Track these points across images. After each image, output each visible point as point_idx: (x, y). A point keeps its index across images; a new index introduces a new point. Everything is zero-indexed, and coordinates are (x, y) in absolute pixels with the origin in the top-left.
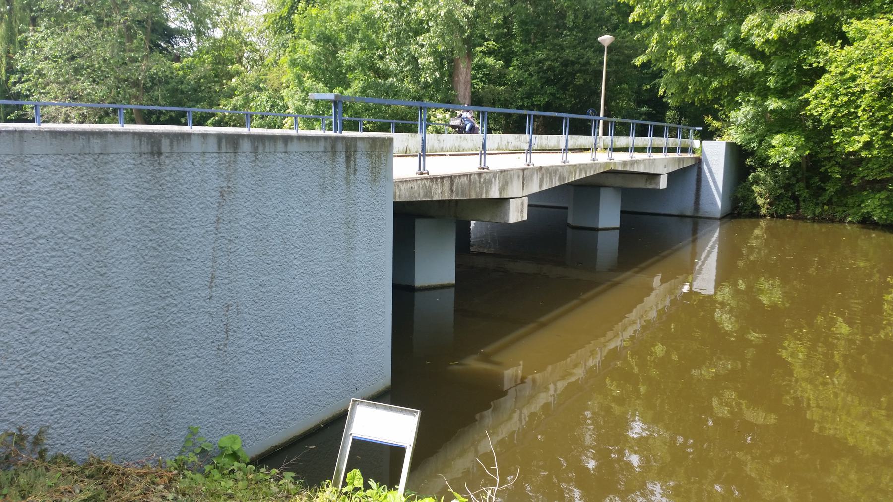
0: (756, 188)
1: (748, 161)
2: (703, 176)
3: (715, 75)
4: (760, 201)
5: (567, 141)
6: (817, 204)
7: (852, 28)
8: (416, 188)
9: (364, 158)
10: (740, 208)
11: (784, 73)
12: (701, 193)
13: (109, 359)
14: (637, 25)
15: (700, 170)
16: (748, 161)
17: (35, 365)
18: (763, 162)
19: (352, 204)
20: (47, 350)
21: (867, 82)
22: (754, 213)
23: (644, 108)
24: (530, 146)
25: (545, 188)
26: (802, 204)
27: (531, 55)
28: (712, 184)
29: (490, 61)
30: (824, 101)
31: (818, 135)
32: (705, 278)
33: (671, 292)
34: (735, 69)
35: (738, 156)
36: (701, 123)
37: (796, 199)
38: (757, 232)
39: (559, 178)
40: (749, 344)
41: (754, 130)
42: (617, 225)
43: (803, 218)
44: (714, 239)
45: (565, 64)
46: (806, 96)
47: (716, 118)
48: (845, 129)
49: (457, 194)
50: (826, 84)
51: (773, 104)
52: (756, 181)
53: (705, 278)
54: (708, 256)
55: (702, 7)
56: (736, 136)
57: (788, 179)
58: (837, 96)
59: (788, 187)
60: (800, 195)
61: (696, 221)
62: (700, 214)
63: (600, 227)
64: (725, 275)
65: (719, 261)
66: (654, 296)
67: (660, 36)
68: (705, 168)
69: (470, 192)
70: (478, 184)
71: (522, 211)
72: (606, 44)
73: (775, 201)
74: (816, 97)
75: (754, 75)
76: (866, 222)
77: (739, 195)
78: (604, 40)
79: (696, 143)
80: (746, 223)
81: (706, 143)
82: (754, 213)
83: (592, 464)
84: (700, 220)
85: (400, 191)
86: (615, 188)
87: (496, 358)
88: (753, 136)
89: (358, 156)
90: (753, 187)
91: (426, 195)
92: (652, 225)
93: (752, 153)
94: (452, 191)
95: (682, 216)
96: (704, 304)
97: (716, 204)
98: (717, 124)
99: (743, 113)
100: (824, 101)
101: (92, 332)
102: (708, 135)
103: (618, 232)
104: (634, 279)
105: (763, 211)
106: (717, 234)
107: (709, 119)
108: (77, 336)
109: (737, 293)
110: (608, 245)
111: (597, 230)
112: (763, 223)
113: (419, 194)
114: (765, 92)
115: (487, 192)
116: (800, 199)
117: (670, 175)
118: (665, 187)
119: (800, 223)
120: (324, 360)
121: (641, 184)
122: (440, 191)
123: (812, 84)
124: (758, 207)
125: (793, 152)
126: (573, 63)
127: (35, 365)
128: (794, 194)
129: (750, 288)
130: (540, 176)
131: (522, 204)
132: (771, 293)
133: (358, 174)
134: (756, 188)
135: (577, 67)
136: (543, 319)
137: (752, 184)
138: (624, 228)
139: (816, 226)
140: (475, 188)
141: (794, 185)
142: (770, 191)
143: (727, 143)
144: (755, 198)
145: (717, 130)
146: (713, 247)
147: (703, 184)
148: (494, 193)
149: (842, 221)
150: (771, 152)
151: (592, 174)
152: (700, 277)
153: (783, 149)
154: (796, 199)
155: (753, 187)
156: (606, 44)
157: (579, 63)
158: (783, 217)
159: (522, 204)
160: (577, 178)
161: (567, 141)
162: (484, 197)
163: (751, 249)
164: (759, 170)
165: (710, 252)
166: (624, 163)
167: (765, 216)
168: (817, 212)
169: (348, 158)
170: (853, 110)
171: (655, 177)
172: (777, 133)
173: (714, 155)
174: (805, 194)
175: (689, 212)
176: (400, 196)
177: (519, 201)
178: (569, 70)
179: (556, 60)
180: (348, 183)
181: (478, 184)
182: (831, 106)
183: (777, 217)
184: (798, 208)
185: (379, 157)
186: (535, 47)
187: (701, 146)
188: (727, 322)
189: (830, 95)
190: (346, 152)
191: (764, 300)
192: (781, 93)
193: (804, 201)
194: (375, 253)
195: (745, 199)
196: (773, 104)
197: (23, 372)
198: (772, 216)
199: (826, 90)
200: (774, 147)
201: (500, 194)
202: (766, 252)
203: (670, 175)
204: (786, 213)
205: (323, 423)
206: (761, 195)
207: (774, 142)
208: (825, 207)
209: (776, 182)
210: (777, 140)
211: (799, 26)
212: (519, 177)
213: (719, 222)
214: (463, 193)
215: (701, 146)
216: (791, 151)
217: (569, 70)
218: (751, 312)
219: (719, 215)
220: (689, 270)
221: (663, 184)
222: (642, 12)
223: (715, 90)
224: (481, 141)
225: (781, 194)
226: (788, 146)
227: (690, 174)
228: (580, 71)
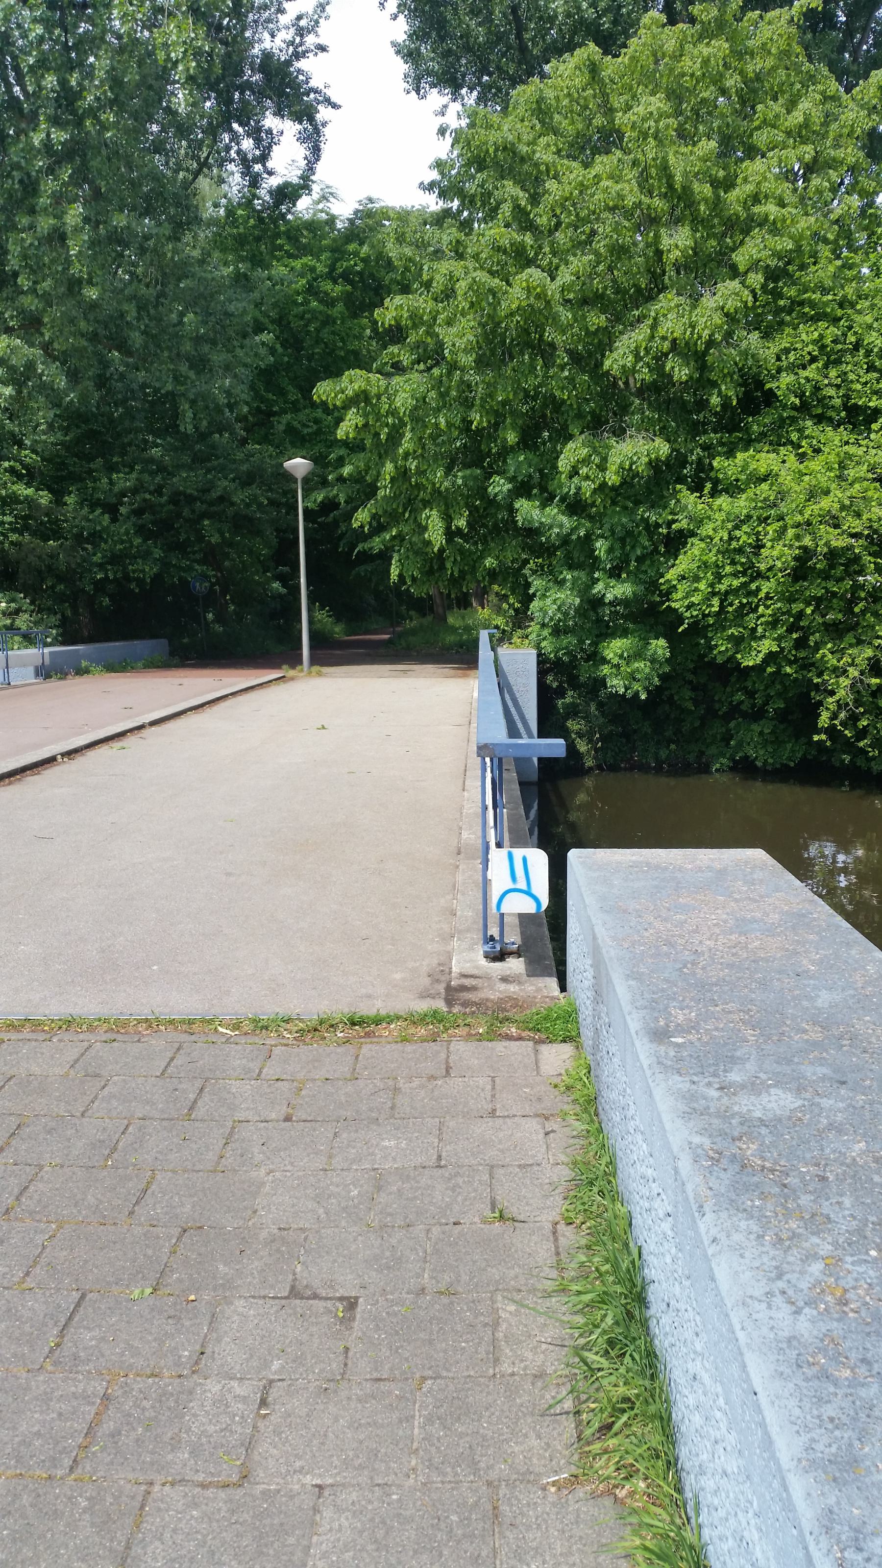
7: (726, 467)
14: (354, 447)
21: (778, 554)
31: (688, 637)
45: (177, 498)
48: (732, 631)
55: (481, 421)
58: (719, 577)
67: (396, 467)
72: (300, 474)
76: (745, 769)
78: (296, 466)
112: (589, 782)
126: (190, 499)
149: (705, 769)
155: (569, 724)
156: (300, 474)
166: (514, 992)
167: (591, 769)
170: (745, 601)
179: (159, 491)
182: (714, 594)
208: (673, 746)
211: (650, 463)
222: (360, 421)
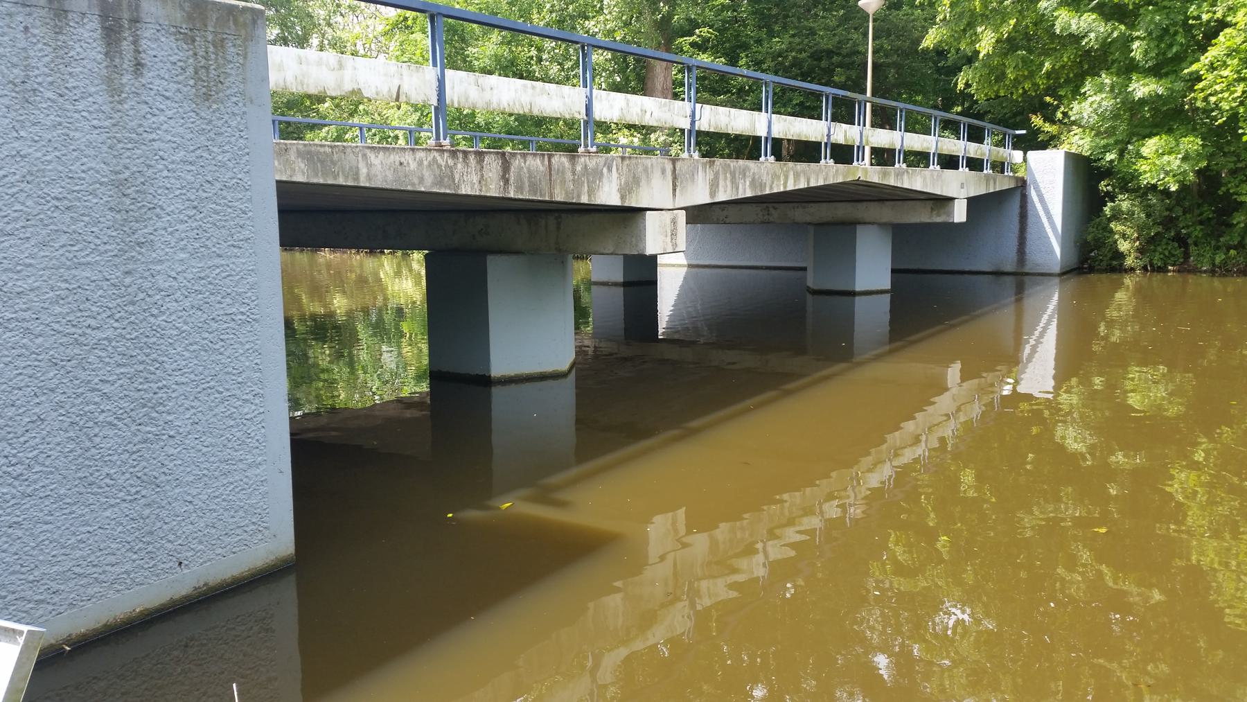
0: (1116, 226)
1: (1103, 186)
2: (1029, 207)
3: (1046, 53)
4: (1124, 246)
5: (770, 123)
6: (1217, 248)
8: (413, 166)
9: (169, 43)
10: (1091, 259)
11: (1162, 35)
12: (1028, 236)
13: (245, 536)
15: (1024, 198)
16: (1103, 186)
17: (150, 548)
18: (1128, 183)
19: (131, 140)
20: (165, 527)
22: (1115, 265)
23: (918, 83)
24: (693, 123)
25: (722, 197)
26: (1192, 248)
27: (766, 45)
28: (1046, 225)
29: (705, 58)
30: (1225, 73)
32: (1038, 375)
33: (982, 390)
34: (1075, 39)
35: (1088, 179)
36: (1026, 124)
37: (1182, 241)
38: (1121, 296)
39: (753, 183)
40: (1111, 474)
41: (1110, 132)
42: (887, 285)
43: (1195, 271)
44: (1049, 312)
46: (1194, 67)
47: (1050, 119)
49: (520, 188)
50: (1228, 44)
51: (1142, 88)
52: (1116, 216)
53: (1038, 375)
54: (1042, 335)
56: (1080, 142)
57: (1170, 209)
59: (1168, 222)
60: (1189, 235)
61: (1020, 279)
62: (1026, 270)
63: (858, 288)
64: (1071, 364)
65: (1059, 336)
66: (953, 400)
68: (1033, 194)
69: (551, 188)
70: (569, 176)
71: (674, 234)
73: (1148, 245)
74: (1212, 68)
75: (1106, 45)
77: (1089, 238)
79: (1017, 156)
80: (1101, 280)
81: (1031, 154)
82: (1115, 265)
83: (1157, 596)
84: (1026, 279)
85: (369, 166)
86: (882, 225)
87: (565, 496)
88: (1111, 141)
89: (147, 33)
90: (1112, 225)
91: (440, 182)
92: (947, 281)
93: (1108, 173)
94: (507, 181)
95: (998, 274)
96: (1042, 415)
97: (1053, 251)
98: (1048, 128)
99: (1093, 102)
100: (1225, 73)
101: (224, 500)
102: (1032, 142)
103: (887, 297)
104: (907, 367)
105: (1129, 262)
106: (1056, 297)
107: (1037, 120)
108: (204, 506)
109: (1092, 397)
110: (872, 316)
111: (853, 294)
112: (1128, 281)
113: (421, 180)
114: (1129, 69)
115: (591, 192)
116: (1189, 241)
117: (973, 202)
118: (964, 219)
119: (1191, 279)
120: (61, 498)
121: (923, 216)
122: (475, 179)
123: (1203, 49)
124: (1121, 256)
125: (1178, 162)
126: (830, 53)
127: (150, 548)
128: (1178, 234)
129: (1111, 386)
130: (710, 175)
131: (674, 222)
132: (1145, 390)
133: (148, 75)
134: (1116, 226)
135: (835, 59)
136: (694, 424)
137: (1110, 220)
138: (896, 292)
139: (1217, 283)
140: (563, 181)
141: (1177, 218)
142: (1140, 229)
143: (1069, 156)
144: (1115, 242)
145: (1053, 138)
146: (1049, 323)
147: (1031, 220)
148: (609, 195)
150: (1142, 166)
151: (821, 183)
152: (1030, 368)
153: (1162, 160)
154: (1182, 241)
155: (1112, 225)
157: (838, 54)
158: (1162, 270)
159: (674, 222)
160: (790, 187)
161: (770, 123)
162: (584, 199)
163: (1111, 324)
164: (1120, 197)
165: (1045, 329)
167: (1132, 269)
168: (1218, 260)
169: (111, 34)
171: (944, 202)
172: (1150, 136)
173: (1047, 173)
174: (1197, 231)
175: (1009, 267)
176: (369, 177)
177: (667, 216)
178: (824, 64)
180: (114, 90)
181: (569, 176)
183: (1153, 270)
184: (1187, 255)
185: (219, 44)
186: (771, 34)
187: (1025, 160)
188: (1073, 439)
189: (1236, 61)
190: (104, 17)
191: (1134, 400)
192: (1156, 71)
193: (1196, 245)
194: (218, 261)
195: (1099, 244)
196: (1142, 88)
197: (135, 557)
198: (1145, 268)
199: (1228, 55)
200: (1145, 158)
201: (623, 198)
202: (1137, 328)
203: (973, 202)
204: (1166, 265)
205: (68, 641)
206: (1124, 236)
207: (1145, 151)
208: (1232, 252)
209: (1148, 216)
210: (1151, 146)
212: (663, 172)
213: (1057, 280)
214: (534, 187)
215: (1025, 160)
216: (1174, 162)
217: (824, 64)
218: (1117, 425)
219: (1057, 270)
220: (1010, 358)
221: (959, 214)
223: (1048, 74)
224: (584, 101)
225: (1156, 234)
226: (1170, 153)
227: (1005, 204)
228: (840, 65)
